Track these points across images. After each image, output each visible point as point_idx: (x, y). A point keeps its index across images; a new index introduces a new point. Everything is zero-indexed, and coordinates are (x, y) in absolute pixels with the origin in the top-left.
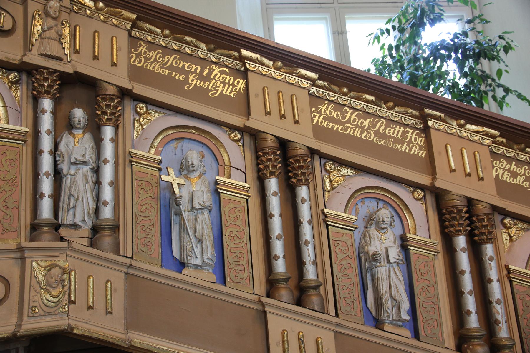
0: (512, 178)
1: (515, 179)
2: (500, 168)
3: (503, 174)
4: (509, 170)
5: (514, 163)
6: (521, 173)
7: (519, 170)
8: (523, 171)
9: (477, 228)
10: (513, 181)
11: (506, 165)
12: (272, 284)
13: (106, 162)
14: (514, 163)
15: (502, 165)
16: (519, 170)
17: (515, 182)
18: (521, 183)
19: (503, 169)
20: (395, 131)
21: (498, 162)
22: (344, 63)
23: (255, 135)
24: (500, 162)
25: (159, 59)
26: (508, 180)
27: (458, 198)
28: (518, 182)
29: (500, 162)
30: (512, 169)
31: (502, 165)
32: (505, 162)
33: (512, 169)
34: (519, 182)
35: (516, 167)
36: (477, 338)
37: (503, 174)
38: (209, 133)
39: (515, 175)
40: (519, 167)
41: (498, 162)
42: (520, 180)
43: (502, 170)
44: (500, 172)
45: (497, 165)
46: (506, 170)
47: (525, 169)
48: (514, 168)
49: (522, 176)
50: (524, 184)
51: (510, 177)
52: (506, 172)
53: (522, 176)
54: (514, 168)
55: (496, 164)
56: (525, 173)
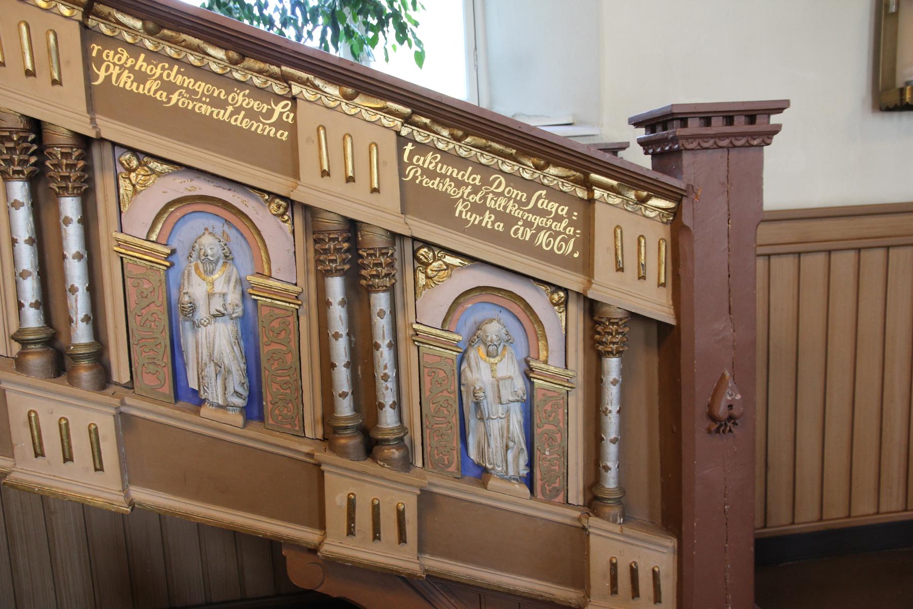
0: (135, 84)
1: (142, 86)
2: (115, 64)
3: (119, 76)
4: (131, 69)
5: (142, 56)
6: (154, 75)
7: (152, 70)
8: (158, 71)
9: (364, 267)
10: (138, 88)
11: (127, 59)
12: (331, 431)
13: (79, 256)
14: (142, 56)
15: (120, 59)
16: (152, 70)
17: (141, 91)
18: (152, 93)
19: (121, 66)
20: (541, 215)
21: (112, 53)
22: (484, 105)
23: (592, 308)
24: (116, 53)
25: (468, 196)
26: (127, 87)
27: (382, 232)
28: (146, 92)
29: (116, 53)
30: (137, 68)
31: (120, 59)
32: (126, 54)
33: (137, 68)
34: (149, 90)
35: (145, 64)
36: (35, 343)
37: (119, 76)
38: (527, 307)
39: (141, 78)
40: (153, 64)
41: (112, 53)
42: (150, 87)
43: (117, 68)
44: (115, 71)
45: (110, 58)
46: (126, 68)
47: (163, 68)
48: (141, 66)
49: (155, 80)
50: (158, 96)
51: (132, 82)
52: (127, 71)
53: (155, 80)
54: (141, 66)
55: (107, 56)
56: (161, 75)
